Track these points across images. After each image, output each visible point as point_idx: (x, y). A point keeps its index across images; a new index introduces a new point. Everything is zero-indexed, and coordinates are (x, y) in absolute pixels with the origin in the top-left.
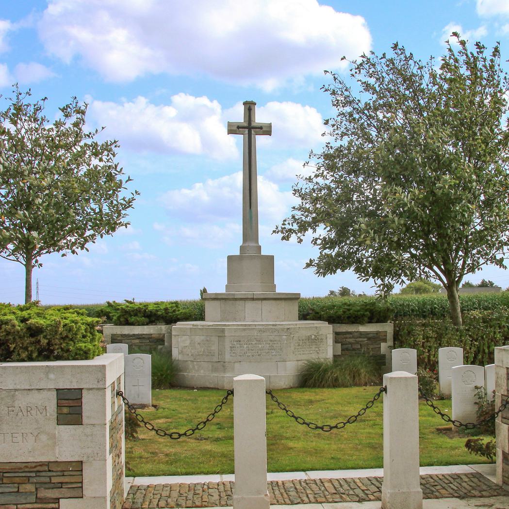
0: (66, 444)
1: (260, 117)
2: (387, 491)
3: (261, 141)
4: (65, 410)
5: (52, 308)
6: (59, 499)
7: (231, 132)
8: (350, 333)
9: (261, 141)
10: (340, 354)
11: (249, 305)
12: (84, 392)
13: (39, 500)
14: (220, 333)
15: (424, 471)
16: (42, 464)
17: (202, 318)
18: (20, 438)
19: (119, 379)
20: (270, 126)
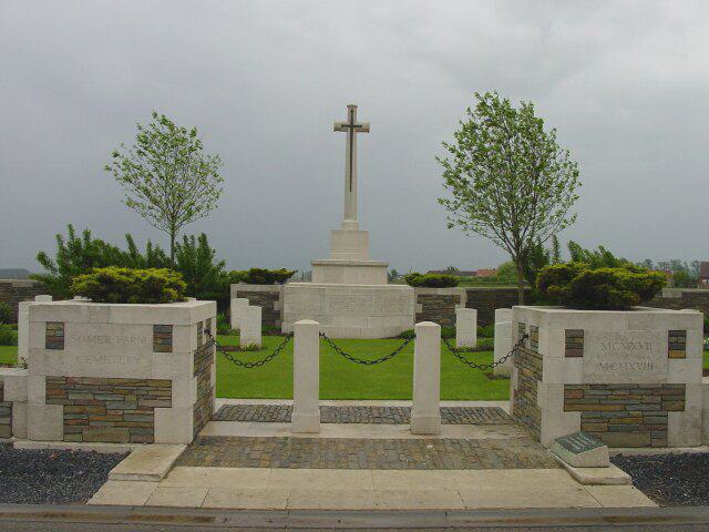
0: (158, 367)
1: (359, 120)
2: (414, 415)
3: (359, 136)
4: (159, 341)
5: (298, 275)
6: (153, 408)
7: (336, 129)
8: (431, 296)
9: (359, 136)
10: (213, 303)
11: (346, 270)
12: (175, 330)
13: (139, 408)
14: (321, 291)
15: (444, 404)
16: (141, 381)
17: (310, 280)
18: (126, 360)
19: (209, 320)
20: (672, 334)
